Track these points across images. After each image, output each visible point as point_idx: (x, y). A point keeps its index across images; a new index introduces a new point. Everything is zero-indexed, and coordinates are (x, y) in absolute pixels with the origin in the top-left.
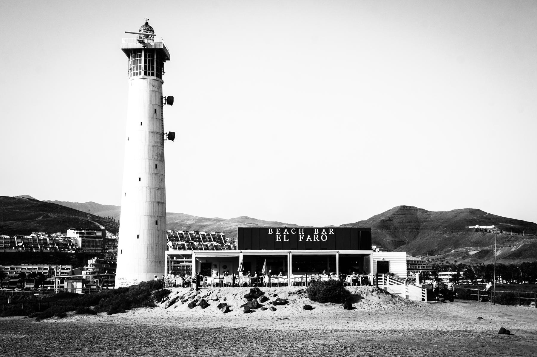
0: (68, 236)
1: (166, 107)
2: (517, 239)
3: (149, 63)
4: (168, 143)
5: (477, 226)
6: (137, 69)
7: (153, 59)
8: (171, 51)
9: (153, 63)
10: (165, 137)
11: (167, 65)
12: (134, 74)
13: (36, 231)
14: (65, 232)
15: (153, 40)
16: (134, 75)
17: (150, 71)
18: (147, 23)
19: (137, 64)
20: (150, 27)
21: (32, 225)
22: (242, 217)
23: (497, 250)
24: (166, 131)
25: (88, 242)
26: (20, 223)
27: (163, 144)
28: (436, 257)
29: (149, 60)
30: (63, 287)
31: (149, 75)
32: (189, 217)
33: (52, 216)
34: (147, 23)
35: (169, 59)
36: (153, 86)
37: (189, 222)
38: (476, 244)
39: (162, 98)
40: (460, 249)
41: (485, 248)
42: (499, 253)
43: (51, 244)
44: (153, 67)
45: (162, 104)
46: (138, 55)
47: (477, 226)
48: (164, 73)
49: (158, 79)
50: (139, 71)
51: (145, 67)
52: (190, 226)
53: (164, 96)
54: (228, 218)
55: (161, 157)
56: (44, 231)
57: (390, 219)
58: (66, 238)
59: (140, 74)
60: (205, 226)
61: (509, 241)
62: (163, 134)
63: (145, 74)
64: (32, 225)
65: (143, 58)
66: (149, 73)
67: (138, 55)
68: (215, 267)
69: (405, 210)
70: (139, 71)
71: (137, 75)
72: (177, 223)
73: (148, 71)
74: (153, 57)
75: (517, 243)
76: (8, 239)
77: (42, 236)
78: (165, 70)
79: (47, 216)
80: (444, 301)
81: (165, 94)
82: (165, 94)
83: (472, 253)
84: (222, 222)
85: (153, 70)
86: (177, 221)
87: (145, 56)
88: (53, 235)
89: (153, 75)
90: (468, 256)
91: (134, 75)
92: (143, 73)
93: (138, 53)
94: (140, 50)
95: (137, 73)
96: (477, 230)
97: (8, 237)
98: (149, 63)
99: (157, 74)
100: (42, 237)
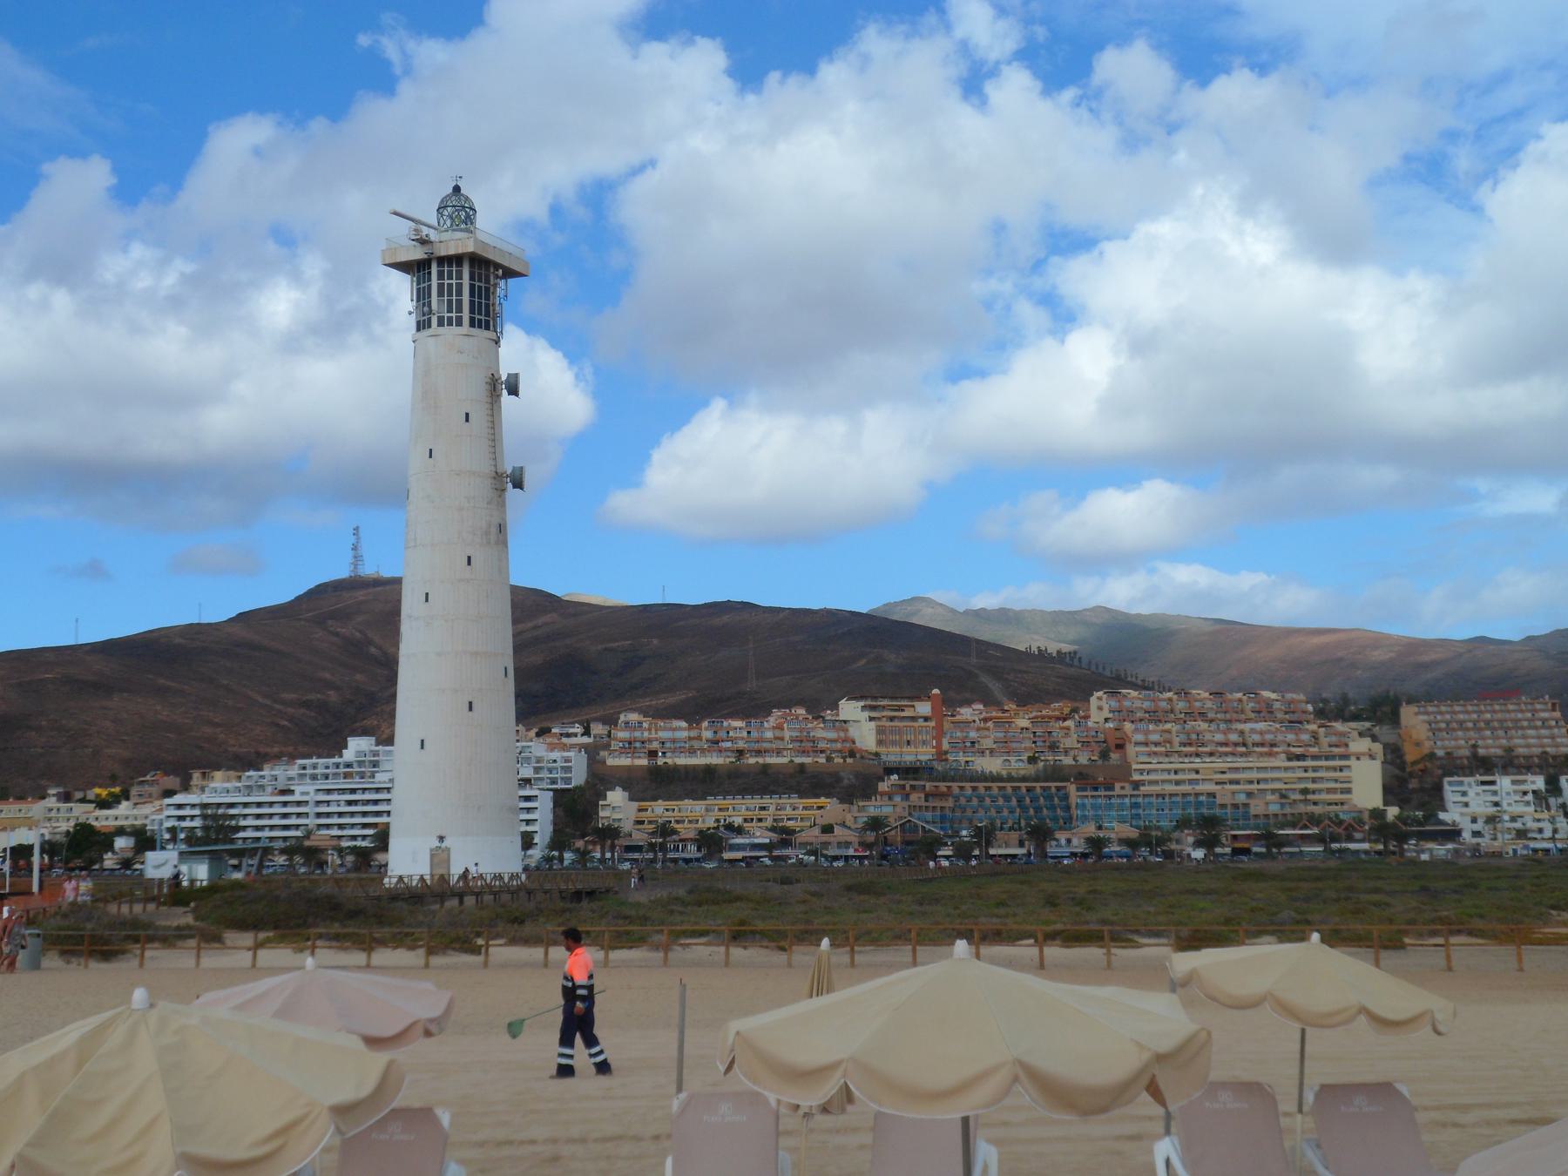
3: (450, 294)
6: (450, 311)
9: (459, 293)
16: (441, 323)
18: (457, 189)
25: (893, 731)
29: (450, 285)
34: (457, 189)
44: (459, 302)
46: (450, 273)
63: (472, 324)
66: (450, 319)
67: (450, 273)
72: (1341, 660)
74: (460, 277)
80: (211, 938)
85: (460, 310)
86: (1340, 654)
87: (472, 278)
89: (459, 323)
92: (466, 320)
93: (450, 265)
95: (450, 319)
98: (450, 294)
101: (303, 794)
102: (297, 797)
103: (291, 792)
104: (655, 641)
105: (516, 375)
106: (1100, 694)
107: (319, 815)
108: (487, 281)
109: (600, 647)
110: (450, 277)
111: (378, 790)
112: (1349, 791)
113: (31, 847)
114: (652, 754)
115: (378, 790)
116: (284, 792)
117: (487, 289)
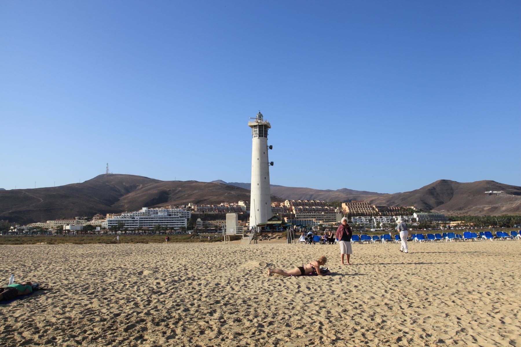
1: (269, 150)
2: (516, 199)
4: (271, 167)
5: (491, 192)
7: (263, 130)
11: (269, 131)
13: (223, 202)
14: (237, 203)
21: (222, 198)
23: (503, 207)
24: (270, 161)
26: (215, 197)
28: (463, 211)
32: (311, 190)
33: (233, 193)
37: (311, 193)
38: (490, 203)
40: (478, 206)
41: (495, 206)
42: (504, 208)
47: (491, 192)
54: (335, 189)
55: (268, 174)
56: (227, 202)
57: (434, 188)
60: (320, 195)
61: (511, 200)
68: (108, 213)
69: (444, 182)
75: (516, 202)
79: (230, 193)
81: (269, 145)
82: (269, 145)
83: (486, 209)
84: (331, 193)
88: (232, 204)
90: (483, 210)
94: (257, 126)
96: (490, 194)
100: (226, 206)
114: (203, 212)
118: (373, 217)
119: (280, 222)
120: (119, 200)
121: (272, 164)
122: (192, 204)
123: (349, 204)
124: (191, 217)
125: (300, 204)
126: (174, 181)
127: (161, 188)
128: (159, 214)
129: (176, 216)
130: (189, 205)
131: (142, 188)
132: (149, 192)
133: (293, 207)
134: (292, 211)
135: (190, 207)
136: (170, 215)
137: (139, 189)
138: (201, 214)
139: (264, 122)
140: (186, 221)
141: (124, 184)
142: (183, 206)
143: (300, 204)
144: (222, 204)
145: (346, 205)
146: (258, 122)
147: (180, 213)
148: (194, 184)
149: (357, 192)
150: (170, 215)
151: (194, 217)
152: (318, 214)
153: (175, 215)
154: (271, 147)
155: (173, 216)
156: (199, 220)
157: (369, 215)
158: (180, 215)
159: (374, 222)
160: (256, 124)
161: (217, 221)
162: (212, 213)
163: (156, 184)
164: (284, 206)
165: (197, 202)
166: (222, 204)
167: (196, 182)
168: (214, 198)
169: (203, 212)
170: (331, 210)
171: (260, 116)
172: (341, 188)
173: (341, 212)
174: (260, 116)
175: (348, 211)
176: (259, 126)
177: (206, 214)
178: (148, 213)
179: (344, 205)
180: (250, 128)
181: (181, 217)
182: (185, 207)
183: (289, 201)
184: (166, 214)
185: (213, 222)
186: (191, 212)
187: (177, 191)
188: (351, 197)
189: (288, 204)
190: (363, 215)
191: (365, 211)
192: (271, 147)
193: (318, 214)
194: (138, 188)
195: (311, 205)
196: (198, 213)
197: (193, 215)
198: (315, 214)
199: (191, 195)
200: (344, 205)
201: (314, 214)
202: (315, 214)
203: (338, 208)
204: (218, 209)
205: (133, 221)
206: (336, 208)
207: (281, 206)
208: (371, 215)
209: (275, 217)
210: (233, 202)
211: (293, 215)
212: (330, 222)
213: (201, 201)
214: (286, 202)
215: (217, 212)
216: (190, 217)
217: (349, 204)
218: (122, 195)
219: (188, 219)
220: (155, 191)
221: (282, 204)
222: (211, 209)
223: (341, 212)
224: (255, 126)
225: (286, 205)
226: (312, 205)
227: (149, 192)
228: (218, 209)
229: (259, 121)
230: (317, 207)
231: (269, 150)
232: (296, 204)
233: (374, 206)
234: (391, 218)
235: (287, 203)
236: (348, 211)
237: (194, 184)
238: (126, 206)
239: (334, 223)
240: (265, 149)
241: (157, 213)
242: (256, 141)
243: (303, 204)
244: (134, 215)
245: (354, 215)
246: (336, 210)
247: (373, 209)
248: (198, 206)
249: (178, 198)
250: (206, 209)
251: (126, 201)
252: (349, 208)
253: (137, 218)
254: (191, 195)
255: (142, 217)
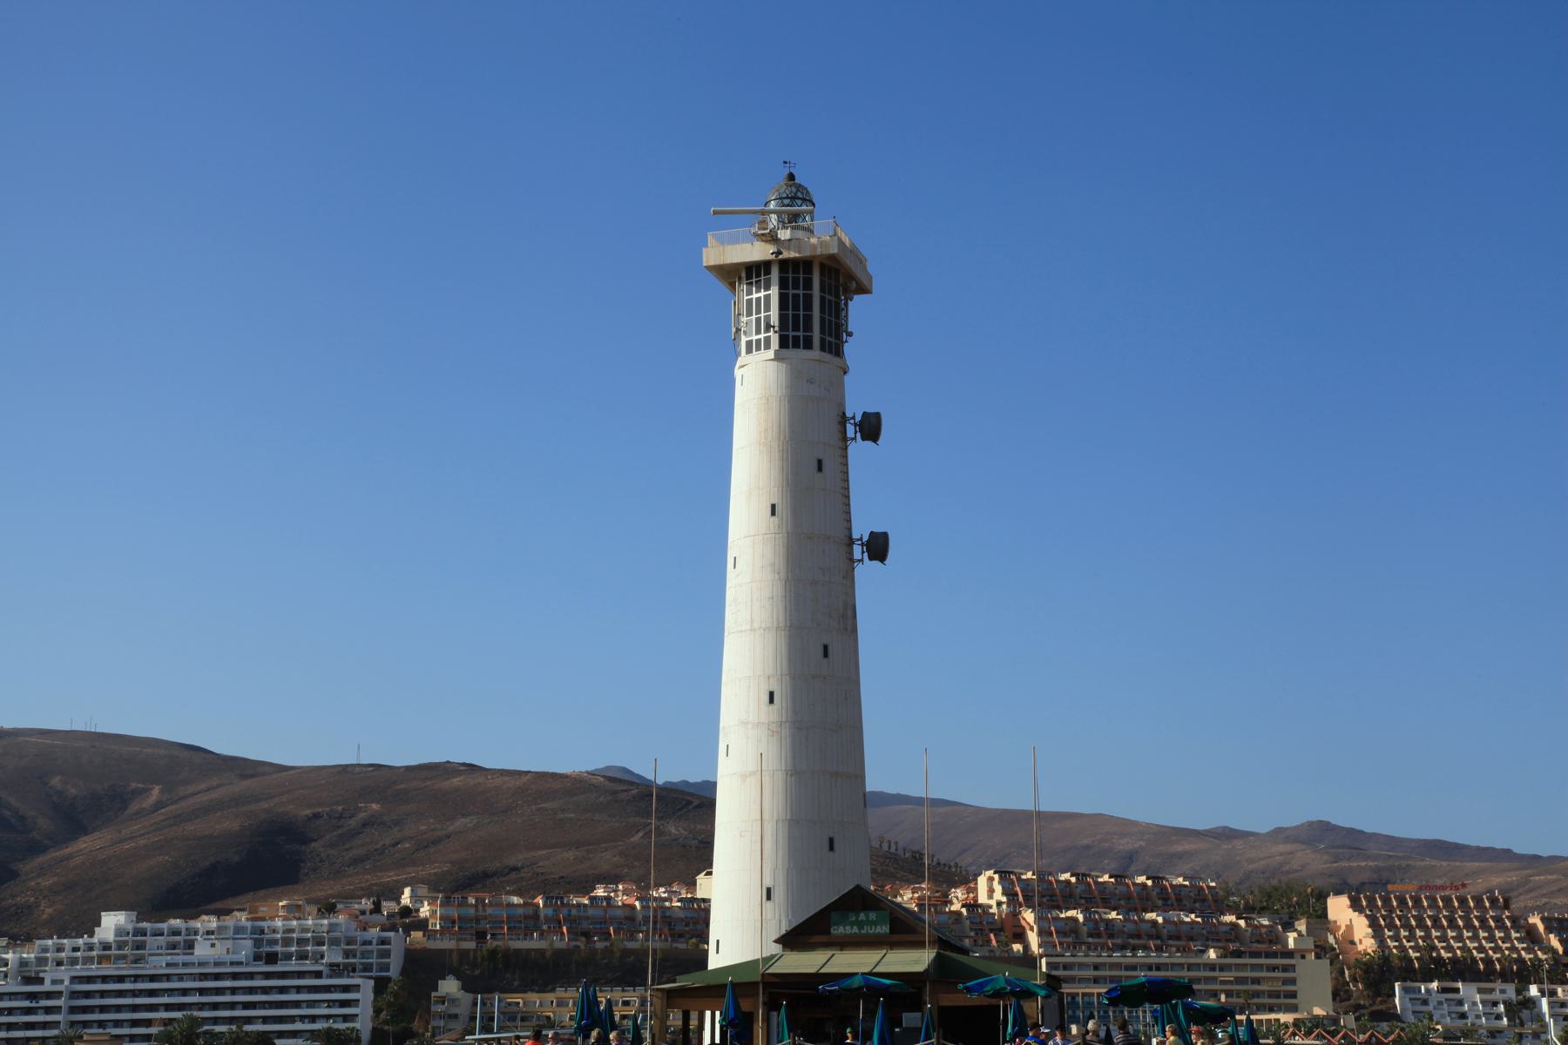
0: (699, 895)
1: (859, 450)
3: (796, 308)
4: (866, 572)
7: (816, 302)
8: (876, 269)
10: (857, 551)
11: (858, 310)
12: (749, 344)
13: (610, 879)
15: (810, 230)
16: (749, 351)
17: (801, 334)
19: (758, 312)
20: (799, 187)
21: (606, 859)
22: (1311, 824)
26: (570, 855)
27: (849, 577)
30: (1390, 1016)
31: (796, 345)
32: (1125, 826)
34: (791, 177)
35: (863, 290)
36: (810, 381)
37: (1125, 845)
39: (843, 420)
43: (548, 920)
44: (808, 319)
45: (845, 439)
46: (796, 281)
48: (850, 334)
49: (827, 357)
50: (762, 336)
51: (783, 318)
52: (1131, 857)
53: (849, 415)
54: (1263, 828)
58: (693, 900)
59: (767, 347)
60: (1180, 856)
62: (851, 542)
64: (606, 859)
65: (774, 292)
66: (796, 339)
67: (796, 281)
70: (762, 336)
71: (758, 349)
72: (1087, 847)
73: (791, 334)
74: (808, 284)
76: (518, 905)
77: (623, 896)
78: (852, 326)
82: (855, 408)
84: (1238, 844)
86: (1085, 842)
89: (808, 345)
91: (749, 351)
93: (758, 275)
95: (758, 341)
97: (516, 900)
98: (796, 308)
99: (822, 341)
100: (621, 899)
101: (54, 982)
102: (47, 986)
103: (41, 981)
104: (374, 806)
105: (877, 415)
106: (990, 873)
107: (73, 1010)
108: (837, 296)
109: (308, 812)
110: (796, 287)
111: (153, 978)
112: (1293, 981)
113: (725, 986)
114: (480, 936)
115: (153, 978)
116: (28, 980)
117: (837, 304)
118: (1534, 990)
119: (916, 960)
120: (14, 875)
121: (878, 547)
122: (423, 890)
123: (1371, 901)
124: (404, 971)
125: (1067, 897)
126: (345, 769)
127: (265, 805)
128: (202, 950)
129: (308, 966)
130: (406, 898)
131: (159, 805)
132: (190, 828)
133: (1029, 916)
134: (1020, 936)
135: (406, 912)
136: (272, 958)
137: (140, 814)
138: (464, 954)
139: (820, 237)
140: (366, 992)
141: (56, 781)
142: (366, 904)
143: (1067, 897)
144: (600, 892)
145: (1355, 905)
146: (772, 238)
147: (334, 942)
148: (456, 781)
149: (1393, 842)
150: (272, 958)
151: (423, 969)
152: (1178, 958)
153: (302, 956)
154: (871, 428)
155: (293, 965)
156: (449, 986)
157: (1505, 976)
158: (333, 956)
159: (1539, 1018)
160: (759, 252)
161: (560, 992)
162: (535, 943)
163: (245, 784)
164: (972, 906)
165: (450, 887)
166: (600, 892)
167: (472, 768)
168: (559, 860)
169: (480, 936)
170: (1259, 936)
171: (796, 197)
172: (1294, 816)
173: (1322, 950)
174: (796, 197)
175: (1366, 943)
176: (784, 265)
177: (493, 953)
178: (134, 943)
179: (1339, 909)
180: (720, 286)
181: (336, 970)
182: (377, 909)
183: (1004, 875)
184: (245, 949)
185: (535, 997)
186: (398, 942)
187: (353, 822)
188: (1360, 867)
189: (999, 895)
190: (1463, 969)
191: (1477, 946)
192: (871, 428)
193: (1178, 958)
194: (134, 807)
195: (1138, 901)
196: (448, 944)
197: (413, 958)
198: (1165, 958)
199: (436, 842)
200: (1339, 909)
201: (1154, 957)
202: (1165, 958)
203: (1302, 926)
204: (570, 920)
205: (32, 996)
206: (1289, 926)
207: (956, 907)
208: (1523, 974)
209: (856, 901)
210: (668, 884)
211: (1029, 960)
212: (1261, 1008)
213: (486, 875)
214: (982, 881)
215: (561, 940)
216: (394, 972)
217: (1371, 901)
218: (36, 849)
219: (381, 985)
220: (229, 823)
221: (958, 897)
222: (530, 922)
223: (1322, 950)
224: (754, 272)
225: (983, 899)
226: (1143, 901)
227: (190, 828)
228: (570, 920)
229: (784, 234)
230: (1173, 915)
231: (859, 450)
232: (1048, 898)
233: (1535, 920)
234: (1511, 991)
235: (989, 891)
236: (1366, 943)
237: (456, 781)
238: (47, 911)
239: (1286, 1018)
240: (824, 444)
241: (190, 946)
242: (757, 381)
243: (1091, 898)
244: (41, 961)
245: (1408, 973)
246: (1291, 938)
247: (1531, 936)
248: (446, 902)
249: (356, 861)
250: (497, 922)
251: (46, 882)
252: (1373, 923)
253: (57, 978)
254: (436, 842)
255: (94, 969)
